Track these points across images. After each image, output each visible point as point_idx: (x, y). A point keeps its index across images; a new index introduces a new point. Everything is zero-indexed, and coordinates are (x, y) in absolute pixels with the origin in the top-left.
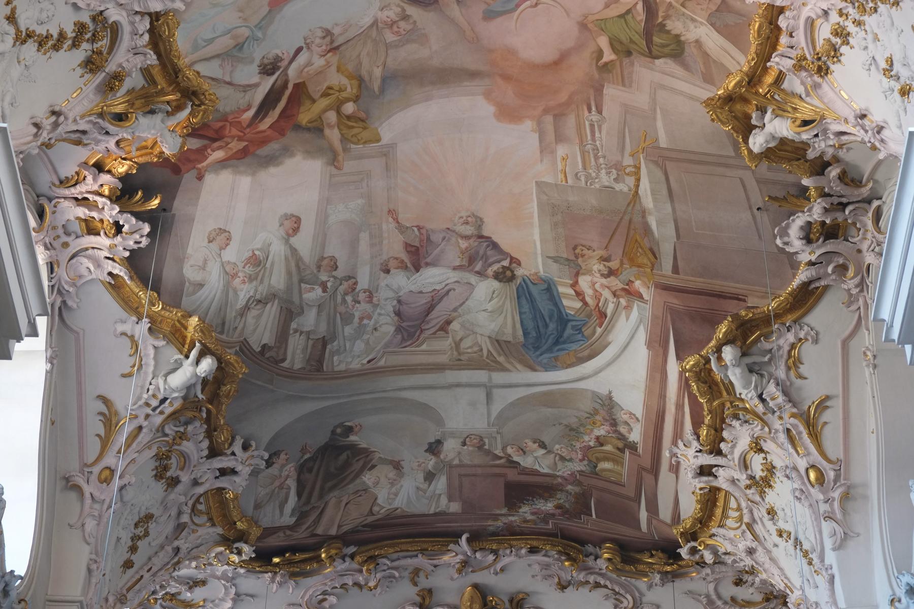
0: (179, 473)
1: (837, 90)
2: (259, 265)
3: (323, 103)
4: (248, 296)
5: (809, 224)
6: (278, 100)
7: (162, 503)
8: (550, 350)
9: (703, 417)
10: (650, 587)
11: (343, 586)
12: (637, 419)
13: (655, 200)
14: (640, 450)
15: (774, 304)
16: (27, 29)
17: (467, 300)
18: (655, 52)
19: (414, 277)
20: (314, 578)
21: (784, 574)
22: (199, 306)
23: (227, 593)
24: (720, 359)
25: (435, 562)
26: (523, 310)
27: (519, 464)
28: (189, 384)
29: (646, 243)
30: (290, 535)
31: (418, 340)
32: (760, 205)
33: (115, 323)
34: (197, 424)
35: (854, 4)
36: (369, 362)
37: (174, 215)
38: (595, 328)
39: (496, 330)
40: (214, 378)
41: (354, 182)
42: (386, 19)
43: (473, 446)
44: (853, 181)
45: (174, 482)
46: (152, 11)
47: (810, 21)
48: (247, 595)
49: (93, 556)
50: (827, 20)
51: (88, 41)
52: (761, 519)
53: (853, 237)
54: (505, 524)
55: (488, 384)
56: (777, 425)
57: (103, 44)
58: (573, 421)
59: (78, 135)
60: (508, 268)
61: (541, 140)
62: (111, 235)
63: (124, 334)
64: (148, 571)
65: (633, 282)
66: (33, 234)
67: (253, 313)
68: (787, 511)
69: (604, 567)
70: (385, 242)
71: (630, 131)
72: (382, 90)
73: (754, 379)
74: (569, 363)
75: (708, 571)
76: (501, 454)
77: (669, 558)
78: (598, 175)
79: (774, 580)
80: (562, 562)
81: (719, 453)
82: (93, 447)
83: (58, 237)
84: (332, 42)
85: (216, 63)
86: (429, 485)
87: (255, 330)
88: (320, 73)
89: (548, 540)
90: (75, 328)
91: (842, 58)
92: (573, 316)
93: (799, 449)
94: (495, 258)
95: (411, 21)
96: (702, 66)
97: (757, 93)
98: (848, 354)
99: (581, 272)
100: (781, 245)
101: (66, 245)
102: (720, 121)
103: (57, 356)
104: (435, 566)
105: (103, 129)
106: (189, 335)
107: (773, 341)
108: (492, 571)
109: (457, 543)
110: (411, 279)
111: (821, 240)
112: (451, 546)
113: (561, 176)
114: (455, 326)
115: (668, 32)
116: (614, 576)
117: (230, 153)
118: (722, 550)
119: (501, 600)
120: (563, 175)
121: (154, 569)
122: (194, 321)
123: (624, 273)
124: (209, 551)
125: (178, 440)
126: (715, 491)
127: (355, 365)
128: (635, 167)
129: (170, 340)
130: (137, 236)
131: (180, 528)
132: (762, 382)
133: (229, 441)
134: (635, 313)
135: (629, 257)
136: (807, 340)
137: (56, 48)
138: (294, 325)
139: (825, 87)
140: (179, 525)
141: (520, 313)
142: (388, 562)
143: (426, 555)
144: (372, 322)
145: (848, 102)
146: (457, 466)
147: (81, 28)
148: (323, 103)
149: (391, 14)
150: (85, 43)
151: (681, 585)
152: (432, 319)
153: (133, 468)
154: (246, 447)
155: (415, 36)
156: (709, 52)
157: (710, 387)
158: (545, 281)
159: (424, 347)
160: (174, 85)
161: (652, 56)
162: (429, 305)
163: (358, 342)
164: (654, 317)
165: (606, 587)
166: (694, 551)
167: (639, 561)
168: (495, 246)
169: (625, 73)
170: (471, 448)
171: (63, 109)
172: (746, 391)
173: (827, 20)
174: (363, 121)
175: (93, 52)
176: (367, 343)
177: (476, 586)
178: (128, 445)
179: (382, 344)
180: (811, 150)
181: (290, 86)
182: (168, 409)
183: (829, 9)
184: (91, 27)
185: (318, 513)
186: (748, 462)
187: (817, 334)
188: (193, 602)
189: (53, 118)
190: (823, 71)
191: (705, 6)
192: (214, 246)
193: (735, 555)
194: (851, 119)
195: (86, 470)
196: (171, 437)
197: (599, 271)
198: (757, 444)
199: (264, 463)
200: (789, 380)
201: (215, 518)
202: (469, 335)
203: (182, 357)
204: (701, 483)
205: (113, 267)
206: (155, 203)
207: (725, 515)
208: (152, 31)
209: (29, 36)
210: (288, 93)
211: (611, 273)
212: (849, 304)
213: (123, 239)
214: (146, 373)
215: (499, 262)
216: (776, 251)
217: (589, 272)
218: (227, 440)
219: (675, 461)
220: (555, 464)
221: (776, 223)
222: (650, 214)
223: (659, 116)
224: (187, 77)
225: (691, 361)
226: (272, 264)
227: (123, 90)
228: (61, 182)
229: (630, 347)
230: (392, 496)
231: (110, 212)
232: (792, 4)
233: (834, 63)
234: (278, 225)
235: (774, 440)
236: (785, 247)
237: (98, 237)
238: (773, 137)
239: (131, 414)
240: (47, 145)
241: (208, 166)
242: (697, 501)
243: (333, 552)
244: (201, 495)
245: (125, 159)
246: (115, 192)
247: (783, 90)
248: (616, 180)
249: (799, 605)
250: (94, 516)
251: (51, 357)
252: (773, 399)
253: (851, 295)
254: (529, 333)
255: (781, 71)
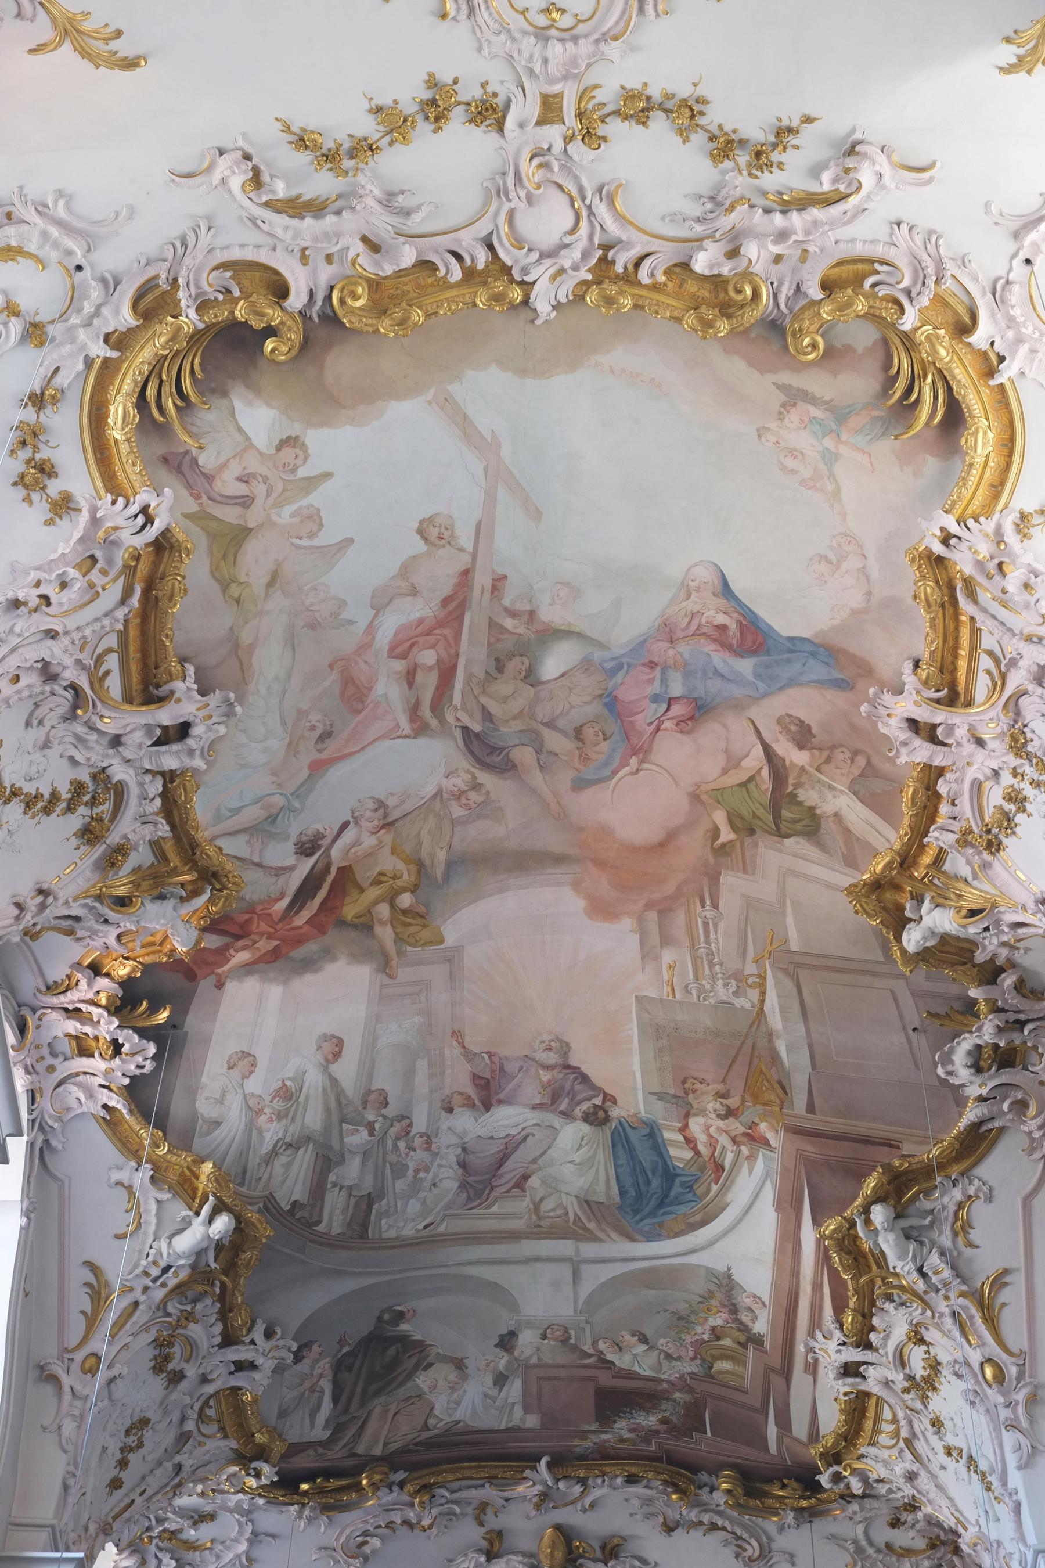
0: (185, 1365)
1: (1012, 870)
2: (290, 1099)
3: (374, 893)
4: (276, 1139)
5: (979, 1047)
6: (318, 888)
7: (162, 1403)
8: (652, 1214)
9: (847, 1298)
10: (781, 1529)
11: (390, 1525)
12: (763, 1303)
13: (784, 1019)
14: (767, 1345)
15: (935, 1152)
16: (13, 785)
17: (549, 1148)
18: (784, 830)
19: (483, 1118)
20: (353, 1513)
21: (955, 1506)
22: (214, 1150)
23: (241, 1532)
24: (868, 1222)
25: (506, 1494)
26: (620, 1162)
27: (614, 1364)
28: (199, 1248)
29: (773, 1074)
30: (321, 1455)
31: (487, 1199)
32: (917, 1025)
33: (110, 1169)
34: (208, 1301)
35: (1031, 761)
36: (425, 1227)
37: (187, 1033)
38: (709, 1184)
39: (586, 1187)
40: (230, 1242)
41: (410, 995)
42: (452, 788)
43: (555, 1339)
44: (1032, 992)
45: (177, 1377)
46: (166, 768)
47: (976, 785)
48: (267, 1535)
49: (71, 1468)
50: (998, 783)
51: (86, 804)
52: (923, 1433)
53: (1034, 1065)
54: (595, 1444)
55: (575, 1259)
56: (943, 1307)
57: (105, 808)
58: (682, 1307)
59: (70, 922)
60: (601, 1108)
61: (642, 943)
62: (108, 1057)
63: (119, 1183)
64: (141, 1494)
65: (757, 1125)
66: (11, 1052)
67: (283, 1159)
68: (957, 1420)
69: (722, 1502)
70: (448, 1072)
71: (752, 931)
72: (447, 877)
73: (911, 1247)
74: (676, 1230)
75: (855, 1507)
76: (591, 1351)
77: (806, 1489)
78: (712, 987)
79: (941, 1514)
80: (669, 1495)
81: (868, 1346)
82: (77, 1327)
83: (43, 1058)
84: (385, 816)
85: (243, 838)
86: (500, 1391)
87: (283, 1182)
88: (370, 855)
89: (650, 1466)
90: (57, 1173)
91: (1018, 830)
92: (683, 1169)
93: (970, 1338)
94: (584, 1095)
95: (484, 791)
96: (842, 846)
97: (911, 876)
98: (1030, 1215)
99: (692, 1112)
100: (943, 1076)
101: (51, 1069)
102: (866, 913)
103: (35, 1209)
104: (507, 1500)
105: (101, 915)
106: (201, 1187)
107: (937, 1199)
108: (579, 1508)
109: (534, 1468)
110: (480, 1121)
111: (994, 1069)
112: (528, 1473)
113: (667, 989)
114: (534, 1182)
115: (800, 804)
116: (736, 1514)
117: (258, 954)
118: (873, 1476)
119: (590, 1546)
120: (670, 988)
121: (149, 1492)
122: (207, 1167)
123: (746, 1113)
124: (220, 1470)
125: (183, 1322)
126: (863, 1397)
127: (408, 1231)
128: (759, 976)
129: (176, 1192)
130: (139, 1059)
131: (183, 1438)
132: (922, 1251)
133: (248, 1325)
134: (760, 1165)
135: (753, 1093)
136: (978, 1197)
137: (47, 811)
138: (332, 1178)
139: (997, 867)
140: (182, 1434)
141: (616, 1166)
142: (447, 1494)
143: (496, 1485)
144: (430, 1176)
145: (1026, 884)
146: (535, 1366)
147: (78, 788)
148: (374, 893)
149: (459, 782)
150: (82, 807)
151: (822, 1526)
152: (505, 1173)
153: (125, 1356)
154: (269, 1334)
155: (487, 810)
156: (851, 828)
157: (856, 1259)
158: (646, 1125)
159: (495, 1209)
160: (190, 864)
161: (781, 834)
162: (501, 1155)
163: (412, 1201)
164: (784, 1169)
165: (724, 1529)
166: (837, 1478)
167: (767, 1495)
168: (584, 1078)
169: (748, 856)
170: (553, 1343)
171: (53, 887)
172: (902, 1263)
173: (998, 783)
174: (422, 917)
175: (92, 818)
176: (424, 1203)
177: (558, 1528)
178: (119, 1325)
179: (443, 1204)
180: (979, 951)
181: (333, 870)
182: (172, 1280)
183: (1000, 768)
184: (91, 787)
185: (358, 1426)
186: (906, 1358)
187: (991, 1190)
188: (198, 1543)
189: (40, 899)
190: (994, 846)
191: (845, 771)
192: (235, 1074)
193: (891, 1482)
194: (1031, 905)
195: (67, 1356)
196: (175, 1317)
197: (715, 1110)
198: (916, 1333)
199: (292, 1356)
200: (956, 1249)
201: (228, 1429)
202: (551, 1194)
203: (191, 1213)
204: (845, 1386)
205: (109, 1098)
206: (163, 1016)
207: (876, 1430)
208: (164, 795)
209: (14, 794)
210: (330, 878)
211: (730, 1113)
212: (1031, 1151)
213: (123, 1061)
214: (146, 1233)
215: (589, 1099)
216: (937, 1084)
217: (702, 1112)
218: (245, 1324)
219: (812, 1358)
220: (660, 1364)
221: (935, 1048)
222: (778, 1037)
223: (789, 910)
224: (206, 854)
225: (831, 1225)
226: (307, 1098)
227: (127, 868)
228: (48, 988)
229: (754, 1210)
230: (452, 1405)
231: (107, 1027)
232: (954, 764)
233: (1007, 836)
234: (315, 1047)
235: (938, 1327)
236: (948, 1078)
237: (92, 1059)
238: (933, 933)
239: (123, 1286)
240: (31, 934)
241: (230, 970)
242: (841, 1411)
243: (377, 1477)
244: (211, 1396)
245: (127, 958)
246: (114, 1002)
247: (944, 873)
248: (736, 994)
249: (975, 1545)
250: (74, 1415)
251: (28, 1210)
252: (936, 1273)
253: (1033, 1140)
254: (626, 1192)
255: (941, 848)
